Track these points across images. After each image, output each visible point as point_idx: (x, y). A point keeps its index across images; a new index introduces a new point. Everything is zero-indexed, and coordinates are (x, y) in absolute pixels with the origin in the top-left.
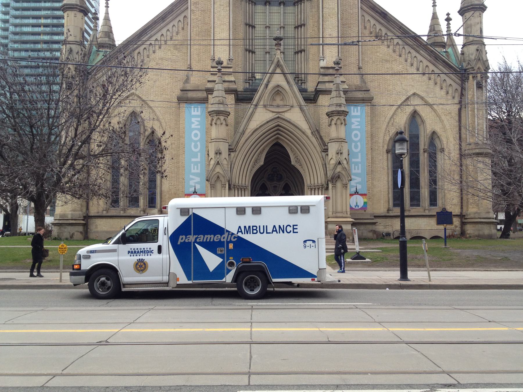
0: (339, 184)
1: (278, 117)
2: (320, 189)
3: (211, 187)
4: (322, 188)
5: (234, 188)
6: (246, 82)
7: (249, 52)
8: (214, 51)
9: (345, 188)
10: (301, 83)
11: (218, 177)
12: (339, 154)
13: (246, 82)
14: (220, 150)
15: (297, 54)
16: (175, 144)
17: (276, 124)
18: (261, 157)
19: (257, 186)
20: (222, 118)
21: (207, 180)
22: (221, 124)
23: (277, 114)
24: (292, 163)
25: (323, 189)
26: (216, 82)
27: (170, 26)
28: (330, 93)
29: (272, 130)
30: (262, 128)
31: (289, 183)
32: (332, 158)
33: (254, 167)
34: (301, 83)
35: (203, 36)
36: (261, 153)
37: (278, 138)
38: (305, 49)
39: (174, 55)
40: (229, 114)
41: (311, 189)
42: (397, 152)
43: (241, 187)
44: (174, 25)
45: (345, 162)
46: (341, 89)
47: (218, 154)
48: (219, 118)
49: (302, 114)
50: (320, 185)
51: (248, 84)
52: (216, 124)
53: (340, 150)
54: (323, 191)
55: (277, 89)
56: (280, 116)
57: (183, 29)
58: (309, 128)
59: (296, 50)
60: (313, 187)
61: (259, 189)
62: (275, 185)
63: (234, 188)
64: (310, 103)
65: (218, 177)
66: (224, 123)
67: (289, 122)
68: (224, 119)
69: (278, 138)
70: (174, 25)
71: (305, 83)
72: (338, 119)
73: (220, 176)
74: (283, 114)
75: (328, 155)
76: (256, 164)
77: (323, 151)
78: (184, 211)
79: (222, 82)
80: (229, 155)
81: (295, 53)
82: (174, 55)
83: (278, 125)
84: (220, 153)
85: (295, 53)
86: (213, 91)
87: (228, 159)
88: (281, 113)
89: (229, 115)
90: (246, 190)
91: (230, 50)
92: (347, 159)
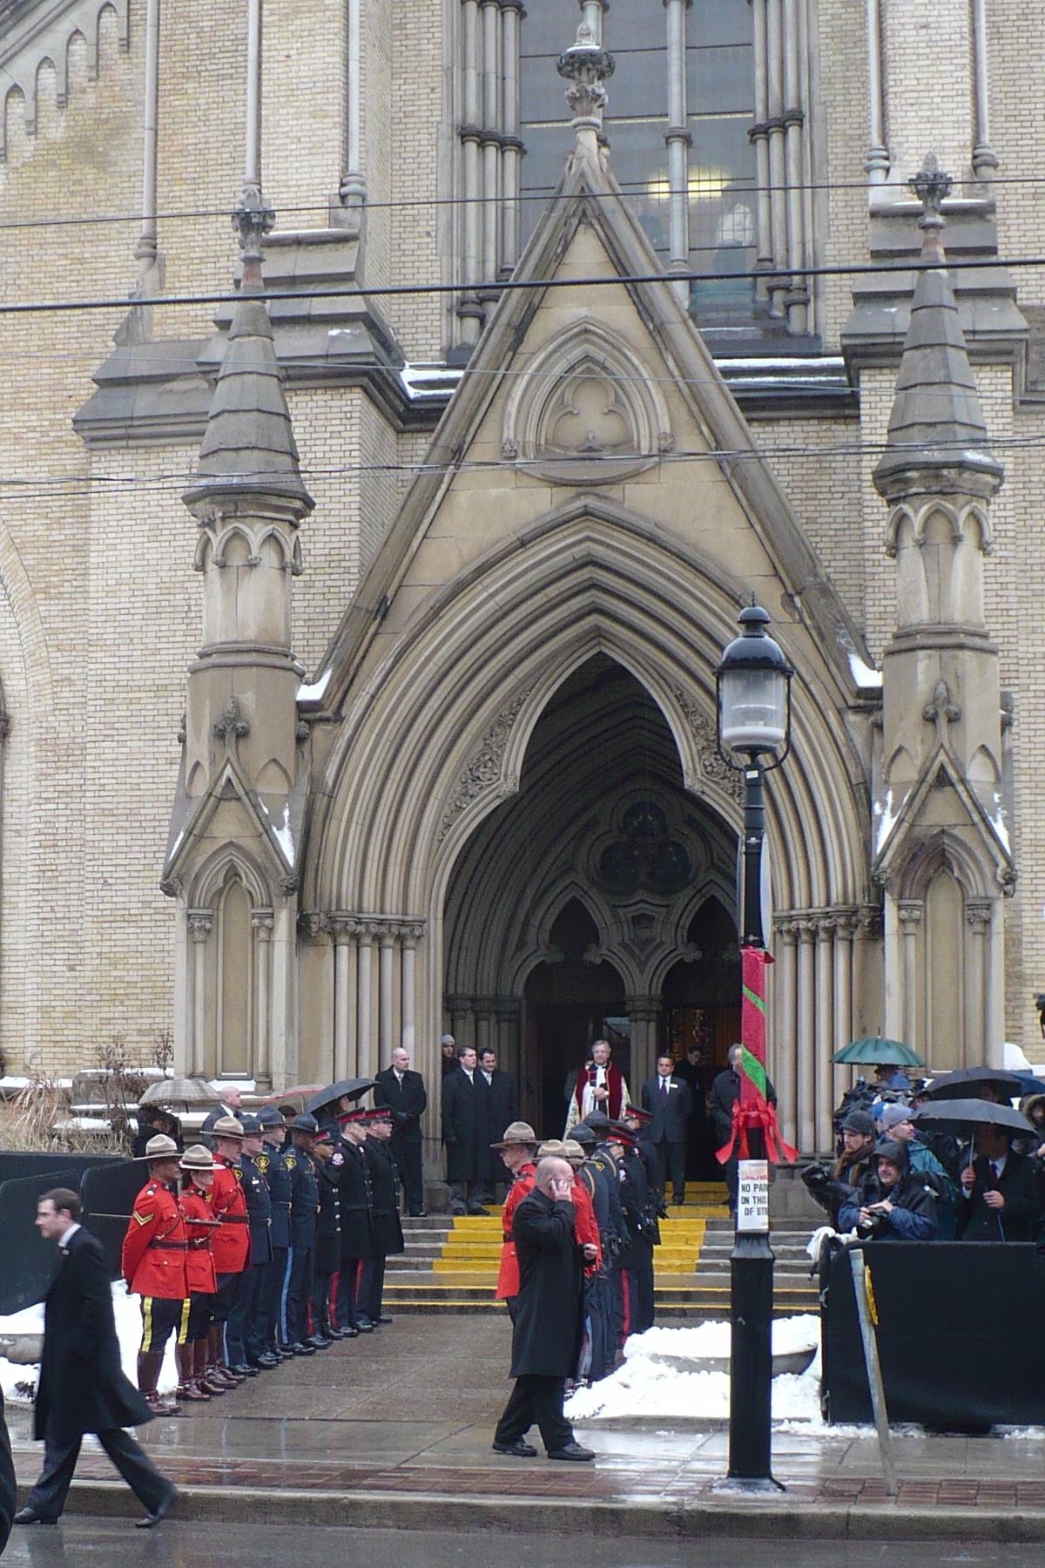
0: (943, 905)
1: (586, 513)
2: (840, 933)
3: (191, 930)
4: (851, 927)
5: (333, 934)
6: (461, 315)
7: (482, 145)
8: (258, 156)
9: (979, 927)
10: (788, 306)
11: (233, 874)
12: (942, 721)
13: (461, 315)
14: (238, 709)
15: (761, 143)
16: (71, 682)
17: (578, 551)
18: (502, 746)
19: (535, 922)
20: (256, 532)
21: (169, 890)
22: (252, 565)
23: (578, 495)
24: (688, 782)
25: (857, 935)
26: (234, 329)
27: (53, 42)
28: (895, 361)
29: (539, 599)
30: (492, 581)
31: (586, 903)
32: (900, 749)
33: (460, 809)
34: (788, 306)
35: (224, 77)
36: (503, 722)
37: (598, 633)
38: (805, 109)
39: (73, 194)
40: (298, 504)
41: (796, 936)
42: (727, 732)
43: (352, 926)
44: (77, 32)
45: (978, 773)
46: (955, 336)
47: (231, 738)
48: (237, 535)
49: (723, 487)
50: (840, 913)
51: (472, 323)
52: (223, 566)
53: (948, 701)
54: (857, 946)
55: (576, 353)
56: (592, 502)
57: (126, 45)
58: (771, 572)
59: (760, 120)
60: (823, 923)
61: (546, 936)
62: (649, 910)
63: (333, 934)
64: (835, 418)
65: (233, 874)
66: (270, 558)
67: (651, 539)
68: (272, 537)
69: (598, 633)
70: (77, 32)
71: (806, 303)
72: (937, 512)
73: (243, 867)
74: (614, 492)
75: (879, 727)
76: (473, 789)
77: (857, 709)
78: (1035, 996)
79: (264, 325)
80: (300, 740)
81: (753, 133)
82: (73, 194)
83: (591, 562)
84: (242, 734)
85: (753, 133)
86: (900, 355)
87: (289, 765)
88: (602, 490)
89: (300, 514)
90: (410, 943)
91: (346, 142)
92: (996, 752)
